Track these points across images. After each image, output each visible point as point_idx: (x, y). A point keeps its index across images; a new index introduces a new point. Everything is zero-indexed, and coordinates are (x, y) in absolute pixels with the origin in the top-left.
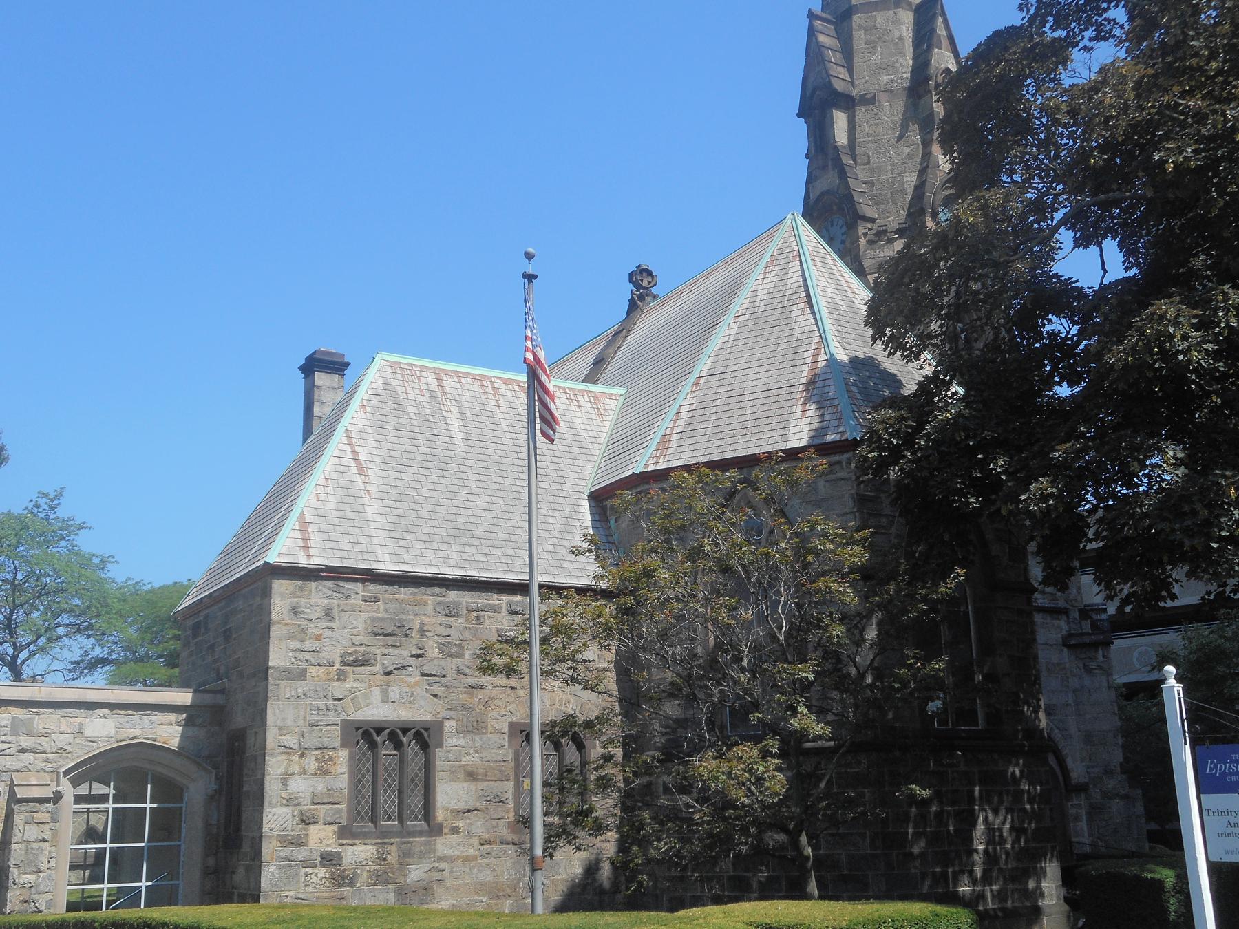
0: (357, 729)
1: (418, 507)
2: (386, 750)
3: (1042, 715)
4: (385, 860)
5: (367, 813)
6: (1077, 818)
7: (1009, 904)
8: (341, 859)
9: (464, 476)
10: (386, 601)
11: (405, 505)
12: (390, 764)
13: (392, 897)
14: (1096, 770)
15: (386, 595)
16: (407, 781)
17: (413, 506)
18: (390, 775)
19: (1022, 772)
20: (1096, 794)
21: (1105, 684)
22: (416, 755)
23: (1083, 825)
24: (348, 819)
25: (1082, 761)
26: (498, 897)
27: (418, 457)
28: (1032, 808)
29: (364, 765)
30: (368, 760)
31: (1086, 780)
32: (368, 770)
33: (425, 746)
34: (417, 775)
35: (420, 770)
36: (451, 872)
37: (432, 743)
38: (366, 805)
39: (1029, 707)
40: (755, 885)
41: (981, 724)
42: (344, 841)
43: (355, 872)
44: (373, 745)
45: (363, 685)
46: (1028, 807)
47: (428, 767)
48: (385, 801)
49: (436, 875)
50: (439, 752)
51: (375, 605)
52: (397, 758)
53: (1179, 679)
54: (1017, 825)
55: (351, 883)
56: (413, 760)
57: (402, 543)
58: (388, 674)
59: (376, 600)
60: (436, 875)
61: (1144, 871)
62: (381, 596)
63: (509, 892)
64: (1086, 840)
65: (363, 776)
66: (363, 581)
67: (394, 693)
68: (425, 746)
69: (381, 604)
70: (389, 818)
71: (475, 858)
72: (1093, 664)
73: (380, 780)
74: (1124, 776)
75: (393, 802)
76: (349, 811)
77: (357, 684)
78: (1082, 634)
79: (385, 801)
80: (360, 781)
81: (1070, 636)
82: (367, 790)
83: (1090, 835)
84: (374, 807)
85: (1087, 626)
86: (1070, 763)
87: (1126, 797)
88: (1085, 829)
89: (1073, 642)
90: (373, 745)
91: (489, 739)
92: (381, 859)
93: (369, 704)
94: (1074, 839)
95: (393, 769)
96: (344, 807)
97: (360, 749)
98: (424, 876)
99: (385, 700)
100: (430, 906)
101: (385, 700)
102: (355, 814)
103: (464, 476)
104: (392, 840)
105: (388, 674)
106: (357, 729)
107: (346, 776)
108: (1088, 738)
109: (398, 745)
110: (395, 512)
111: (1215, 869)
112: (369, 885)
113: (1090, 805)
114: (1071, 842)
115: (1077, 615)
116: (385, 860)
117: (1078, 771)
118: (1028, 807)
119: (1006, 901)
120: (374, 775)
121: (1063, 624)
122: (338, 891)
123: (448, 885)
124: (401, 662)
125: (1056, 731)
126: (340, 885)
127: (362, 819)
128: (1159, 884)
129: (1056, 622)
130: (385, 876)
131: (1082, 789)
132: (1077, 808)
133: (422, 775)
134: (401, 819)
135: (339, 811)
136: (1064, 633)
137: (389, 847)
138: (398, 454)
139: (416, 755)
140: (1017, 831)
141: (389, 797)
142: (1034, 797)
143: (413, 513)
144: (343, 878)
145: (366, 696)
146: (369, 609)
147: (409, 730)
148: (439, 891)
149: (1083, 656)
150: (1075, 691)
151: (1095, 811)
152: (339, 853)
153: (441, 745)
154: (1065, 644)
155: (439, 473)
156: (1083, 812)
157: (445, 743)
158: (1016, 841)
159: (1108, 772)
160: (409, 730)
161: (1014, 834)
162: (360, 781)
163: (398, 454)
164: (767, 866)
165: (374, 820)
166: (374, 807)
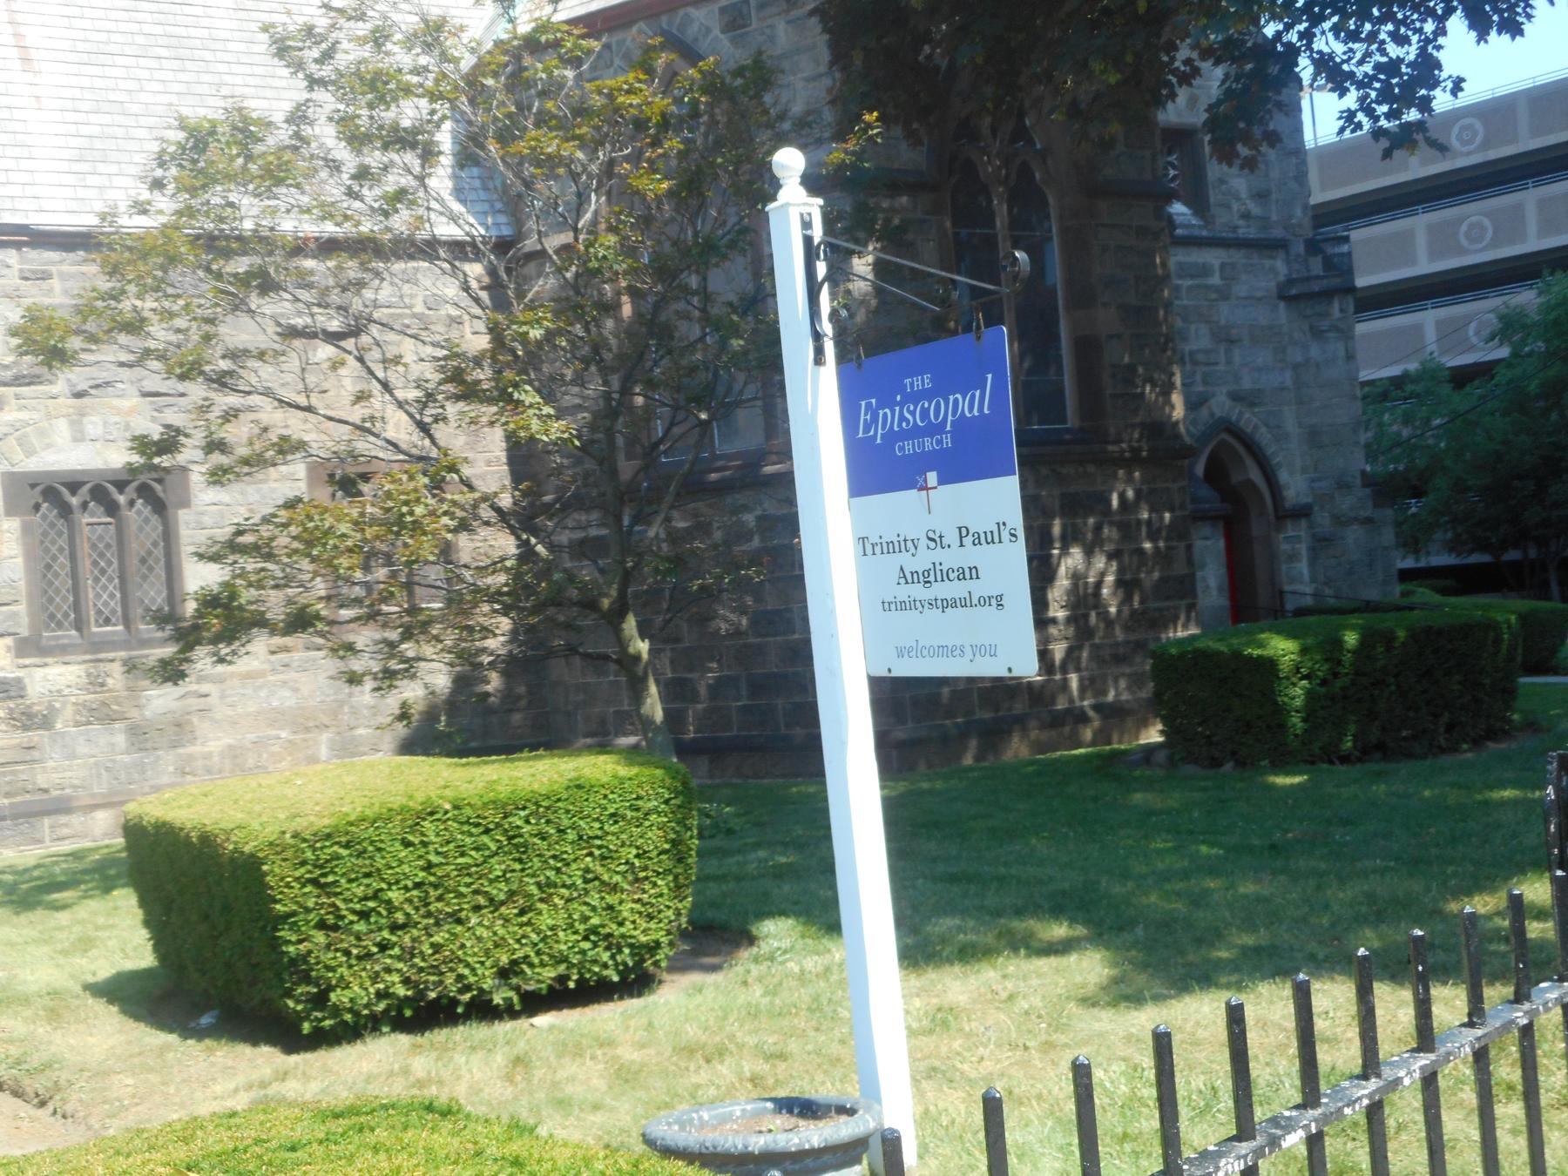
0: (33, 486)
1: (130, 121)
2: (91, 520)
3: (1177, 398)
4: (102, 685)
5: (66, 615)
6: (1293, 557)
7: (1111, 696)
8: (23, 688)
9: (223, 68)
10: (64, 277)
11: (107, 119)
12: (101, 538)
13: (120, 739)
14: (1323, 484)
15: (65, 268)
16: (133, 562)
17: (119, 119)
18: (102, 555)
19: (1138, 493)
20: (1323, 520)
21: (1342, 353)
22: (147, 520)
23: (1303, 567)
24: (32, 626)
25: (1304, 470)
26: (307, 730)
27: (140, 40)
28: (1156, 548)
29: (53, 542)
30: (60, 534)
31: (1309, 500)
32: (61, 550)
33: (160, 507)
34: (150, 553)
35: (155, 544)
36: (223, 696)
37: (170, 499)
38: (64, 603)
39: (1154, 385)
40: (703, 691)
41: (1072, 420)
42: (27, 661)
43: (51, 707)
44: (65, 511)
45: (36, 416)
46: (1147, 545)
47: (169, 538)
48: (98, 596)
49: (194, 703)
50: (183, 515)
51: (45, 285)
52: (111, 527)
53: (812, 183)
54: (1128, 577)
55: (46, 723)
56: (141, 529)
57: (92, 180)
58: (79, 395)
59: (45, 276)
60: (194, 703)
61: (1248, 644)
62: (53, 269)
63: (326, 720)
64: (1308, 590)
65: (54, 558)
66: (18, 246)
67: (94, 426)
68: (160, 507)
69: (56, 283)
70: (107, 621)
71: (262, 674)
72: (1324, 324)
73: (85, 565)
74: (1368, 491)
75: (112, 596)
76: (31, 614)
77: (24, 415)
78: (1308, 279)
79: (98, 596)
80: (48, 567)
81: (1290, 282)
82: (63, 582)
83: (1313, 579)
84: (76, 606)
85: (1316, 266)
86: (1283, 476)
87: (1368, 521)
88: (1305, 571)
89: (1294, 292)
90: (65, 511)
91: (273, 490)
92: (96, 683)
93: (49, 446)
94: (1287, 588)
95: (108, 546)
96: (21, 608)
97: (44, 517)
98: (173, 705)
99: (79, 437)
100: (190, 749)
101: (79, 437)
102: (47, 615)
103: (223, 68)
104: (111, 655)
105: (79, 395)
106: (33, 486)
107: (20, 561)
108: (1313, 437)
109: (112, 508)
110: (84, 130)
111: (896, 700)
112: (77, 724)
113: (1314, 536)
114: (1281, 593)
115: (1301, 249)
116: (102, 685)
117: (1295, 486)
118: (1147, 545)
119: (1105, 693)
120: (73, 557)
121: (1280, 266)
122: (20, 737)
123: (218, 716)
124: (103, 375)
125: (1263, 430)
126: (25, 728)
127: (60, 625)
128: (1268, 666)
129: (1268, 263)
130: (105, 710)
131: (1302, 513)
132: (1294, 543)
133: (159, 552)
134: (127, 622)
135: (14, 615)
136: (1281, 278)
137: (109, 666)
138: (103, 37)
139: (147, 520)
140: (1126, 585)
141: (105, 588)
142: (1159, 530)
143: (120, 132)
144: (29, 715)
145: (43, 433)
146: (34, 291)
147: (80, 484)
148: (202, 726)
149: (1309, 312)
150: (1296, 367)
151: (1321, 544)
152: (19, 680)
153: (185, 503)
154: (1281, 297)
155: (176, 64)
156: (1303, 548)
157: (194, 501)
158: (1127, 599)
159: (1342, 485)
160: (80, 484)
161: (1120, 594)
162: (48, 567)
163: (103, 37)
164: (719, 661)
165: (79, 625)
166: (76, 606)
